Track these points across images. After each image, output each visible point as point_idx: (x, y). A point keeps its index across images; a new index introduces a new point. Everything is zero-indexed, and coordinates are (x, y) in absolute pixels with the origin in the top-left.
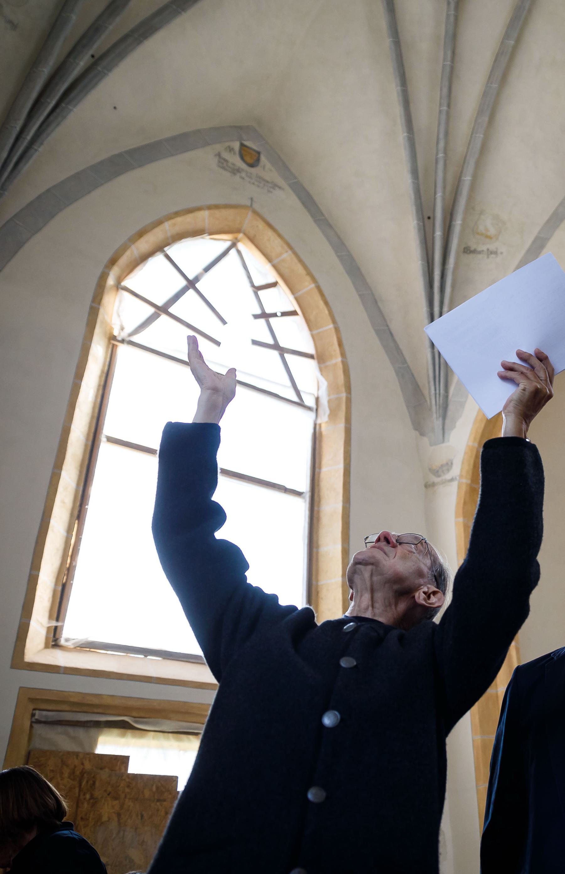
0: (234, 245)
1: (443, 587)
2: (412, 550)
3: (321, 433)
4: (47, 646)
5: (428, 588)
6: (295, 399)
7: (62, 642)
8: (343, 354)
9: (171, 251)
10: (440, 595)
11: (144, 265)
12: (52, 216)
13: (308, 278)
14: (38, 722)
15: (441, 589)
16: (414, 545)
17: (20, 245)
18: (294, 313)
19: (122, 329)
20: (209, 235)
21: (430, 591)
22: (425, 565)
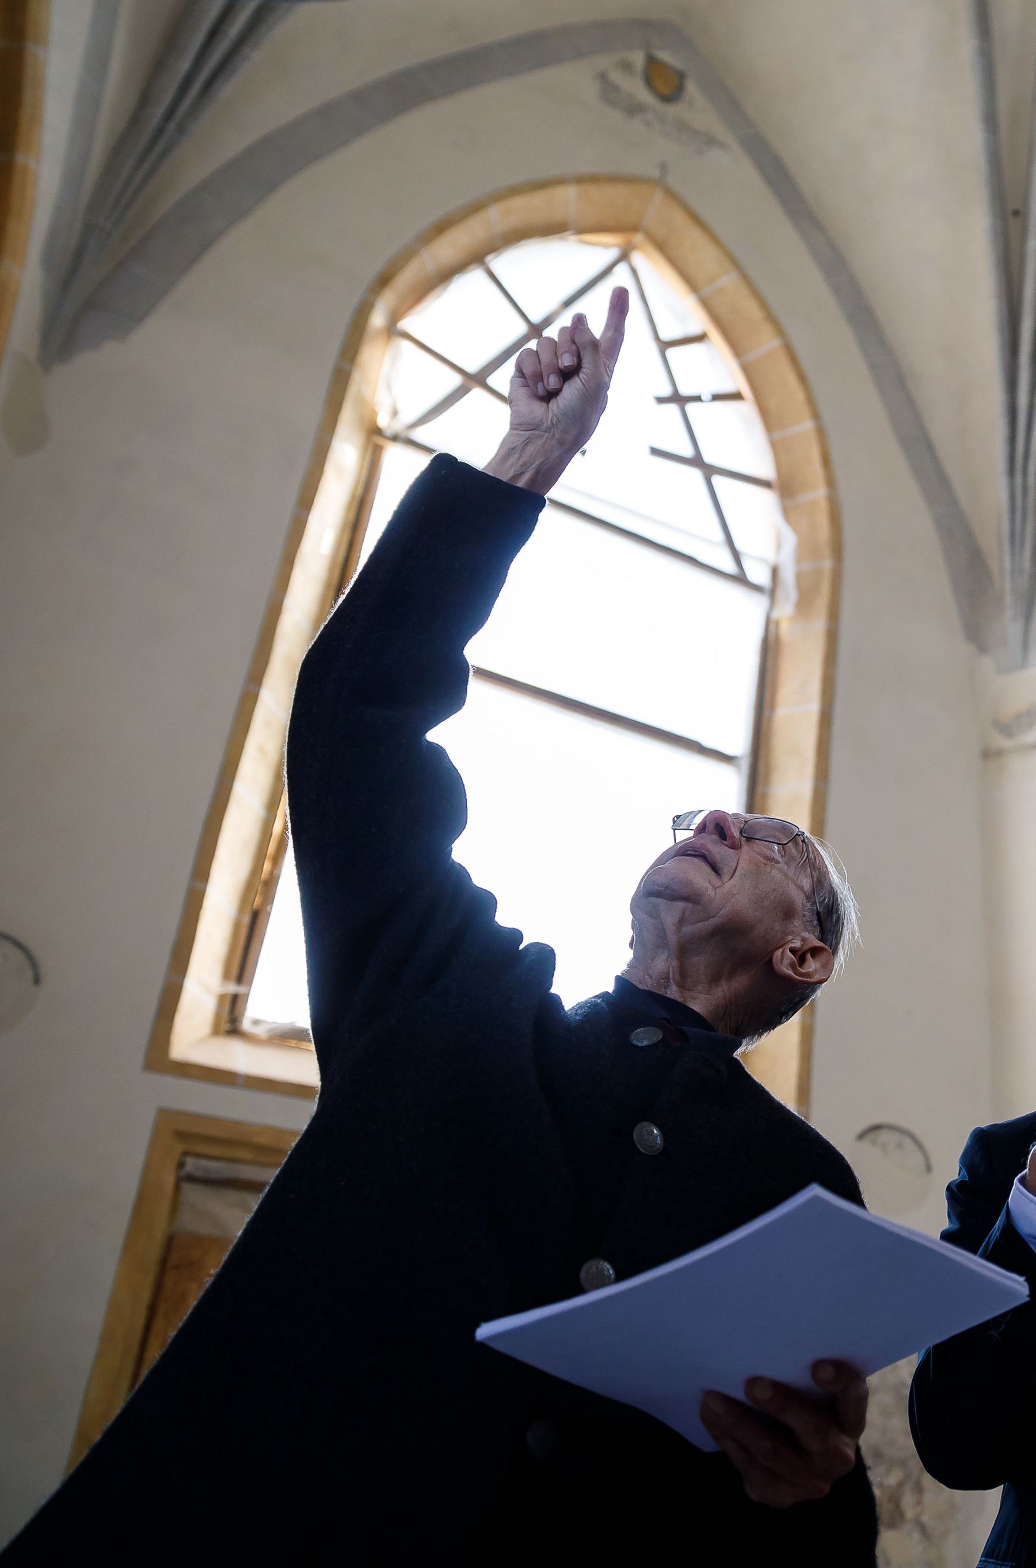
0: (624, 256)
1: (834, 936)
2: (773, 855)
3: (777, 639)
4: (216, 1031)
5: (804, 940)
6: (729, 567)
7: (246, 1025)
8: (831, 483)
9: (499, 263)
10: (823, 957)
11: (445, 289)
12: (272, 186)
13: (767, 330)
14: (191, 1179)
15: (829, 942)
16: (780, 846)
17: (205, 245)
18: (737, 396)
19: (395, 413)
20: (574, 234)
21: (806, 947)
22: (801, 888)
